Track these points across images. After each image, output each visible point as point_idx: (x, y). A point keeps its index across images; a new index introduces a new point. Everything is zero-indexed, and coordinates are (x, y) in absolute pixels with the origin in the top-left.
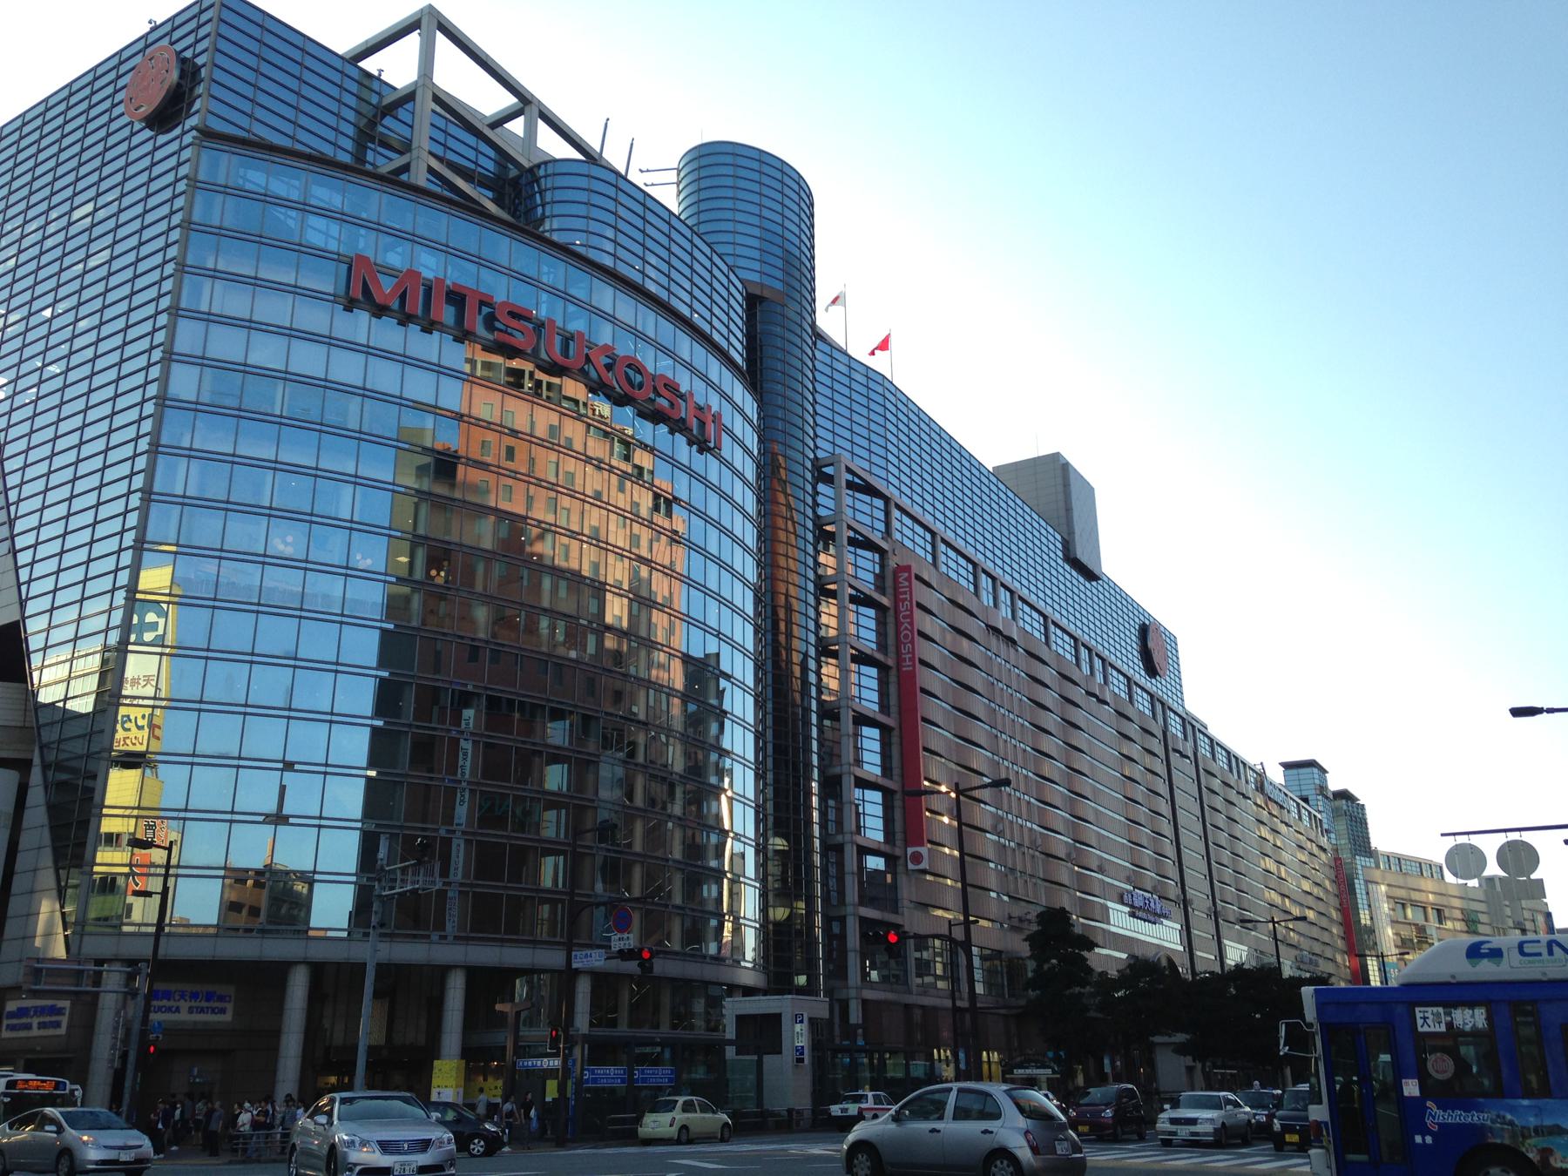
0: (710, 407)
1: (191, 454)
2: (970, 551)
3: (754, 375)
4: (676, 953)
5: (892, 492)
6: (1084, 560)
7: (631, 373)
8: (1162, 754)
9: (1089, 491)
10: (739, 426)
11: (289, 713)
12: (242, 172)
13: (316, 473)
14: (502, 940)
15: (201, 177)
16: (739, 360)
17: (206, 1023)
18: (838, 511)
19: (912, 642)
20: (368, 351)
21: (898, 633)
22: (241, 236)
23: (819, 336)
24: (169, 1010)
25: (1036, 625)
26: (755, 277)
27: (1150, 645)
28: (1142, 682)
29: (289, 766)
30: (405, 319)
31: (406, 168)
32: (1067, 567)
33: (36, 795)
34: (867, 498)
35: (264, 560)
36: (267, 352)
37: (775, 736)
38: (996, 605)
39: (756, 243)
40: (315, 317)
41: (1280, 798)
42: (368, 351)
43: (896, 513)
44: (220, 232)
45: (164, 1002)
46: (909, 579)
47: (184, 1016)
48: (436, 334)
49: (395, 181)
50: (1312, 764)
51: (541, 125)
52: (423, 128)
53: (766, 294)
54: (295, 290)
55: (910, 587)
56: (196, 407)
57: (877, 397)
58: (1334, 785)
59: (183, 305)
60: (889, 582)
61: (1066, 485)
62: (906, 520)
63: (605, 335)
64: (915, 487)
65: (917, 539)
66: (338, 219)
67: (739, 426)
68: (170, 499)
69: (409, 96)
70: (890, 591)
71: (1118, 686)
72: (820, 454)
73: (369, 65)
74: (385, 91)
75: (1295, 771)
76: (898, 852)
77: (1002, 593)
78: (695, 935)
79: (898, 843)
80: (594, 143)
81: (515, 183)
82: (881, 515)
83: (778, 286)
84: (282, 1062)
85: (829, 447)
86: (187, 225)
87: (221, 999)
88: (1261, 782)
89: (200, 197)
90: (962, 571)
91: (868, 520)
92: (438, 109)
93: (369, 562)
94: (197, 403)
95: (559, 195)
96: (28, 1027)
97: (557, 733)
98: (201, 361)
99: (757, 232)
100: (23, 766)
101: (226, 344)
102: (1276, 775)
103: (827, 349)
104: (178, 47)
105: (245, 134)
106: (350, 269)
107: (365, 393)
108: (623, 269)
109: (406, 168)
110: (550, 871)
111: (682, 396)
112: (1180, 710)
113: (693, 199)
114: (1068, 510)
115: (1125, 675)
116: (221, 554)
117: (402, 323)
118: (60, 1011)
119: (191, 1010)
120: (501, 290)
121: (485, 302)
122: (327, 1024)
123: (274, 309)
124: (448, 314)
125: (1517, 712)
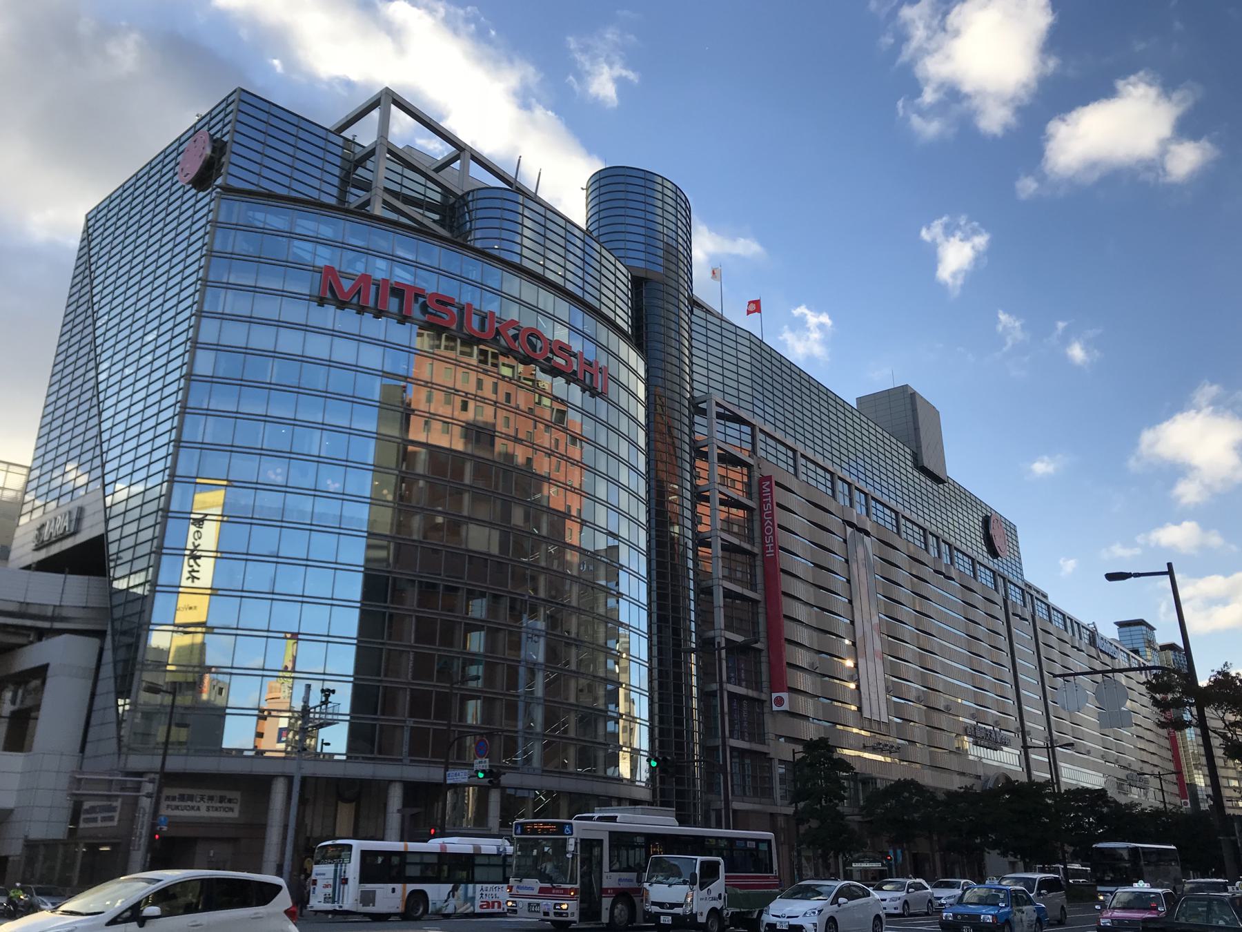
0: (597, 363)
1: (208, 412)
4: (571, 774)
5: (757, 421)
6: (931, 468)
7: (534, 340)
8: (1003, 618)
9: (936, 413)
11: (273, 596)
12: (250, 213)
13: (294, 423)
16: (625, 327)
18: (710, 436)
19: (773, 534)
21: (762, 528)
22: (246, 258)
23: (694, 303)
24: (193, 808)
26: (641, 264)
27: (991, 532)
28: (985, 562)
29: (295, 636)
30: (361, 310)
31: (367, 203)
32: (916, 474)
33: (108, 656)
34: (737, 426)
35: (316, 493)
36: (262, 338)
37: (659, 609)
38: (851, 506)
39: (642, 239)
40: (295, 312)
41: (1111, 650)
42: (333, 333)
44: (231, 256)
45: (189, 803)
46: (770, 486)
47: (203, 813)
48: (382, 320)
49: (362, 213)
50: (1140, 623)
52: (381, 172)
53: (649, 276)
54: (282, 294)
55: (771, 492)
56: (212, 380)
59: (206, 309)
60: (755, 489)
61: (914, 410)
64: (818, 420)
66: (321, 243)
68: (193, 445)
69: (372, 153)
70: (756, 495)
71: (963, 565)
72: (696, 394)
74: (358, 149)
75: (1127, 629)
76: (764, 697)
78: (585, 758)
79: (765, 690)
81: (452, 206)
82: (749, 439)
83: (661, 270)
84: (267, 848)
85: (705, 389)
86: (211, 254)
87: (230, 801)
88: (1093, 637)
89: (219, 234)
91: (737, 443)
93: (337, 485)
95: (480, 214)
96: (95, 820)
97: (478, 609)
98: (217, 348)
100: (100, 634)
101: (235, 335)
102: (1109, 632)
103: (703, 315)
104: (212, 132)
106: (378, 289)
109: (367, 203)
110: (473, 711)
111: (575, 355)
112: (1020, 583)
113: (596, 209)
114: (917, 429)
116: (256, 486)
117: (358, 313)
118: (113, 809)
119: (208, 809)
120: (431, 285)
121: (419, 294)
123: (266, 308)
124: (393, 304)
125: (1111, 577)
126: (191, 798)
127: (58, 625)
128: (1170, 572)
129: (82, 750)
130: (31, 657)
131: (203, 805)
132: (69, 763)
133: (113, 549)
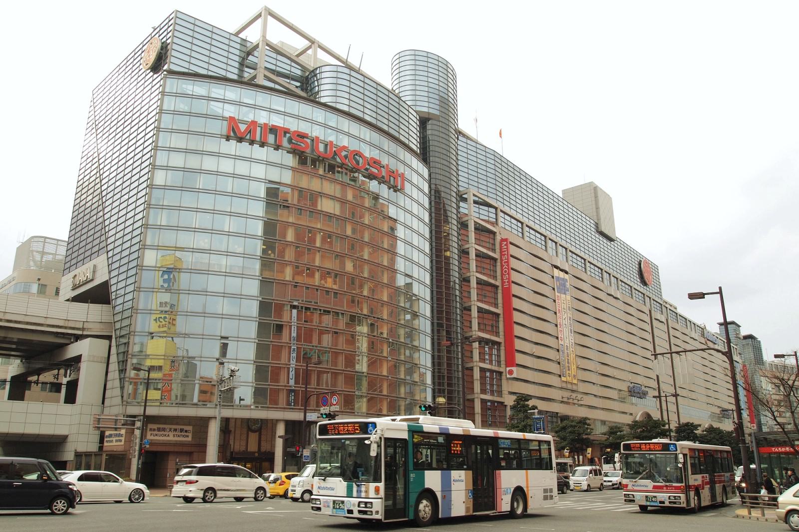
2: (582, 254)
3: (424, 155)
9: (609, 199)
10: (415, 179)
14: (268, 407)
15: (167, 90)
16: (415, 148)
17: (180, 441)
20: (236, 158)
21: (502, 270)
23: (459, 133)
25: (627, 290)
26: (426, 110)
32: (597, 236)
34: (486, 208)
42: (236, 158)
43: (588, 264)
45: (163, 433)
46: (506, 245)
49: (251, 84)
51: (319, 50)
55: (507, 248)
56: (165, 188)
57: (505, 171)
58: (744, 332)
59: (159, 145)
61: (596, 197)
62: (532, 232)
63: (345, 141)
65: (513, 226)
67: (415, 179)
73: (242, 35)
77: (560, 249)
80: (344, 56)
87: (186, 431)
90: (579, 263)
92: (268, 48)
94: (165, 186)
96: (111, 441)
99: (426, 89)
101: (177, 160)
103: (464, 140)
104: (161, 37)
105: (186, 71)
107: (234, 176)
108: (379, 124)
109: (255, 77)
115: (642, 293)
118: (122, 436)
122: (231, 442)
126: (164, 430)
127: (85, 333)
128: (720, 292)
129: (103, 403)
130: (73, 350)
131: (171, 434)
132: (97, 410)
133: (113, 288)
